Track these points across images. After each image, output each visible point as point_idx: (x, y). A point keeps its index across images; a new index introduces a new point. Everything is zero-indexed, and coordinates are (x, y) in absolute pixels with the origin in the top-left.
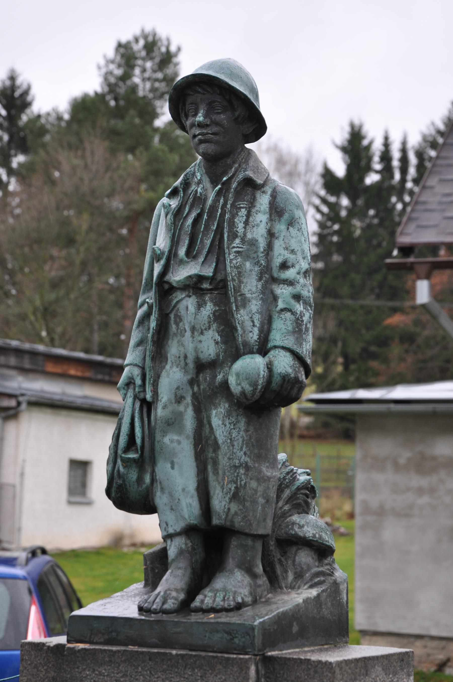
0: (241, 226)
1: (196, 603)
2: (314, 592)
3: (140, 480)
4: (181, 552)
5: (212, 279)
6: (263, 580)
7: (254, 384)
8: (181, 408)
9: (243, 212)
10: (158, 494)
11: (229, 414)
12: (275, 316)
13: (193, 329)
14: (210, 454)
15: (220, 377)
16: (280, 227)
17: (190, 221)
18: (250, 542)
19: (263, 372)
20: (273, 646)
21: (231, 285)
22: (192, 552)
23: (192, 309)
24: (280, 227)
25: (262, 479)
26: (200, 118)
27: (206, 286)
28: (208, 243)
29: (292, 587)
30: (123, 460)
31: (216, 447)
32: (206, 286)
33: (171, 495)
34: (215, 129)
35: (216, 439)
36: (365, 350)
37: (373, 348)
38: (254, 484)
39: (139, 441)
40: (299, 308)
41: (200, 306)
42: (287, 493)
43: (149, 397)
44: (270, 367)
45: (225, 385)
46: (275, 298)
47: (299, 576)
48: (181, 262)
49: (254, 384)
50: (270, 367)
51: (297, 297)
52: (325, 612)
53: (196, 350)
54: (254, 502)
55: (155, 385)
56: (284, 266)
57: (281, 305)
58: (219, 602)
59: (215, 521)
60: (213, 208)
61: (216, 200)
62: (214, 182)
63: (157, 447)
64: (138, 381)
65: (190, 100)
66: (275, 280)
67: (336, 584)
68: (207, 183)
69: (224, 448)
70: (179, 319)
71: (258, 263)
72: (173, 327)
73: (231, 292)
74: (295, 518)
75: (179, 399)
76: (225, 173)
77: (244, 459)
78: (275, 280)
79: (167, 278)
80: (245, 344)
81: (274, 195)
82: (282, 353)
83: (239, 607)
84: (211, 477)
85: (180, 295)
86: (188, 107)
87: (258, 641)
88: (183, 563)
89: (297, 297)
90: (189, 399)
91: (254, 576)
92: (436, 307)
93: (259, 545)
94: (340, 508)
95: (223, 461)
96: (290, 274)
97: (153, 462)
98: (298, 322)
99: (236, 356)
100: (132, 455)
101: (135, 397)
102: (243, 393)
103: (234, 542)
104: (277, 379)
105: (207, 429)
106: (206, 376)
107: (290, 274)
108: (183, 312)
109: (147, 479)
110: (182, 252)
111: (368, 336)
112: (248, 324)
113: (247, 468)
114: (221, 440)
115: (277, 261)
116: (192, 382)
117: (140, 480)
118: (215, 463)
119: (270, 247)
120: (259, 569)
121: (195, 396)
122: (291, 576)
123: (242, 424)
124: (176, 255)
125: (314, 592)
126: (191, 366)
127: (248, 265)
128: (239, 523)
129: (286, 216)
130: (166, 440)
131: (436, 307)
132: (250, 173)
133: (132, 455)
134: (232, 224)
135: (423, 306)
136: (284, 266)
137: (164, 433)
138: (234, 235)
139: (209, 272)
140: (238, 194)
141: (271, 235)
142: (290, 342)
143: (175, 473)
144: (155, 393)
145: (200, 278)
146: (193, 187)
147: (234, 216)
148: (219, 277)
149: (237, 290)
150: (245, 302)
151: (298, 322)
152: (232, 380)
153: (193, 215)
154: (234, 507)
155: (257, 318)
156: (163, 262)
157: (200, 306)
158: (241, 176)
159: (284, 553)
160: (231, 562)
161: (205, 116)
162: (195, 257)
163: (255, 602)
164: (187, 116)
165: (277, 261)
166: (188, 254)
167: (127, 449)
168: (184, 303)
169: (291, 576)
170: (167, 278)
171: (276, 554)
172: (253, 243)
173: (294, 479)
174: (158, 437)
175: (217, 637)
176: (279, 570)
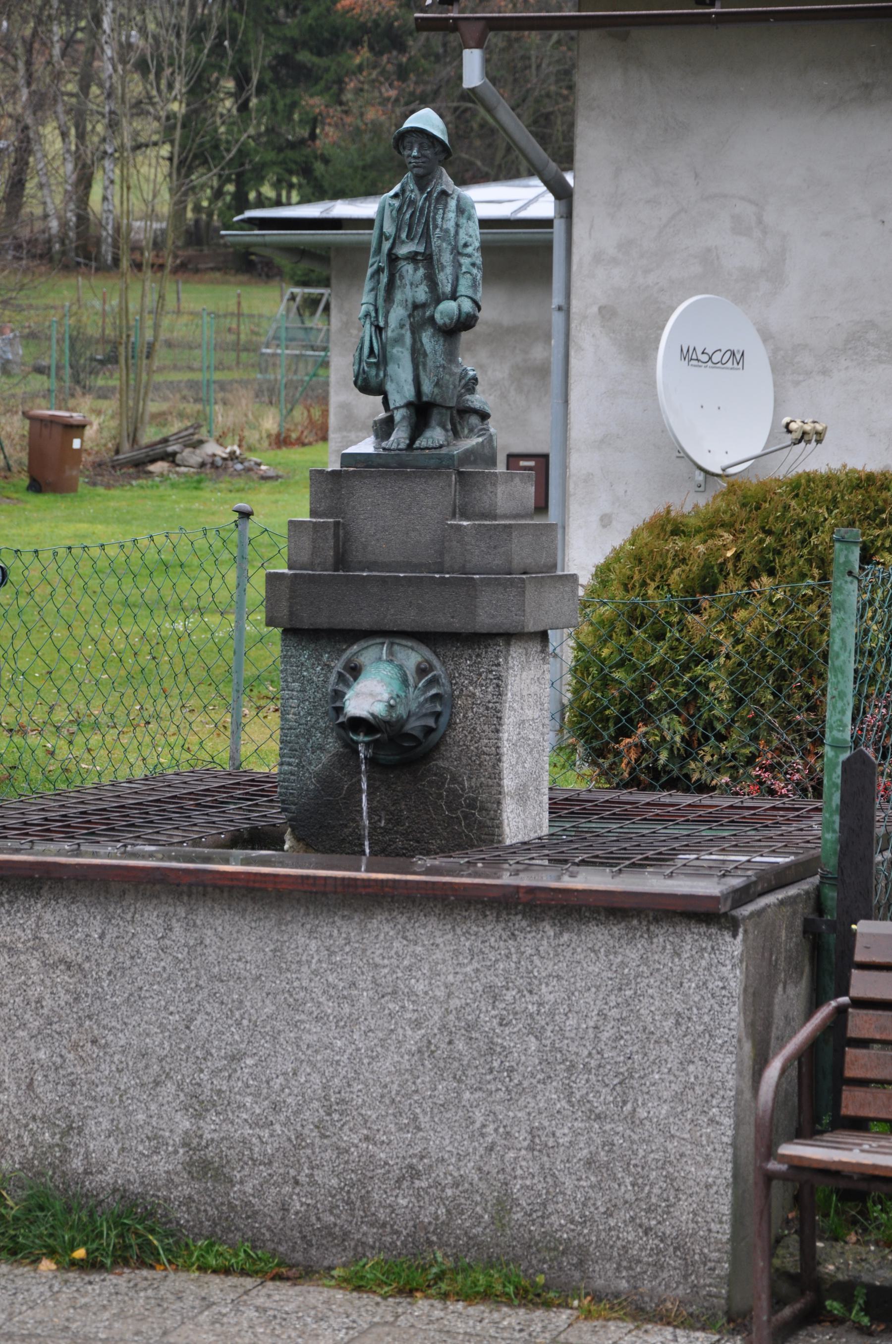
0: (439, 221)
1: (417, 444)
2: (480, 440)
3: (377, 375)
4: (404, 418)
5: (423, 254)
6: (450, 433)
7: (451, 319)
8: (403, 331)
9: (441, 211)
10: (389, 383)
11: (433, 336)
12: (461, 276)
13: (412, 284)
14: (421, 359)
15: (428, 313)
16: (463, 221)
17: (408, 216)
18: (444, 411)
19: (456, 312)
20: (462, 466)
21: (435, 258)
22: (410, 417)
23: (411, 271)
24: (463, 221)
25: (452, 374)
26: (415, 153)
27: (419, 258)
28: (420, 230)
29: (467, 437)
30: (367, 363)
31: (425, 355)
32: (419, 258)
33: (398, 384)
34: (424, 160)
35: (425, 351)
36: (283, 60)
37: (304, 56)
38: (447, 377)
39: (376, 351)
40: (475, 271)
41: (416, 270)
42: (463, 382)
43: (382, 324)
44: (459, 306)
45: (432, 319)
46: (460, 265)
47: (471, 430)
48: (403, 242)
49: (451, 319)
50: (459, 306)
51: (473, 265)
52: (486, 451)
53: (413, 297)
54: (447, 387)
55: (386, 317)
56: (466, 245)
57: (464, 269)
58: (430, 444)
59: (425, 399)
60: (422, 208)
61: (424, 203)
62: (422, 189)
63: (388, 355)
64: (373, 314)
65: (407, 140)
66: (459, 254)
67: (491, 436)
68: (417, 191)
69: (430, 356)
70: (402, 277)
71: (450, 244)
72: (398, 282)
73: (435, 262)
74: (468, 397)
75: (402, 326)
76: (427, 184)
77: (443, 362)
78: (459, 254)
79: (394, 251)
80: (444, 293)
81: (458, 201)
82: (466, 299)
83: (441, 447)
84: (422, 373)
85: (403, 263)
86: (406, 143)
87: (456, 463)
88: (405, 423)
89: (473, 265)
90: (408, 326)
91: (446, 430)
92: (492, 94)
93: (449, 412)
94: (256, 427)
95: (430, 364)
96: (469, 250)
97: (386, 364)
98: (474, 280)
99: (438, 301)
100: (373, 360)
101: (372, 324)
102: (445, 324)
103: (435, 411)
104: (463, 316)
105: (419, 345)
106: (419, 312)
107: (469, 250)
108: (404, 273)
109: (382, 374)
110: (404, 236)
111: (292, 25)
112: (445, 281)
113: (444, 367)
114: (428, 350)
115: (462, 242)
116: (410, 316)
117: (377, 375)
118: (424, 365)
119: (457, 233)
120: (449, 427)
121: (411, 324)
122: (466, 431)
123: (441, 342)
124: (399, 237)
125: (480, 440)
126: (410, 306)
127: (444, 245)
128: (439, 400)
129: (466, 214)
130: (395, 351)
131: (492, 94)
132: (444, 187)
133: (373, 360)
134: (434, 219)
135: (473, 90)
136: (466, 245)
137: (393, 347)
138: (436, 227)
139: (421, 249)
140: (438, 200)
141: (457, 225)
142: (470, 293)
143: (400, 371)
144: (386, 323)
145: (417, 253)
146: (408, 193)
147: (435, 214)
148: (428, 252)
149: (439, 260)
150: (443, 268)
151: (474, 280)
152: (437, 316)
153: (410, 212)
154: (436, 391)
155: (450, 277)
156: (391, 241)
157: (416, 270)
158: (439, 189)
159: (461, 418)
160: (433, 423)
161: (418, 152)
162: (412, 240)
163: (448, 445)
164: (404, 148)
165: (462, 242)
166: (407, 237)
167: (369, 357)
168: (406, 268)
169: (466, 431)
170: (394, 251)
171: (457, 419)
172: (447, 231)
173: (467, 374)
174: (389, 349)
175: (432, 461)
176: (459, 427)
